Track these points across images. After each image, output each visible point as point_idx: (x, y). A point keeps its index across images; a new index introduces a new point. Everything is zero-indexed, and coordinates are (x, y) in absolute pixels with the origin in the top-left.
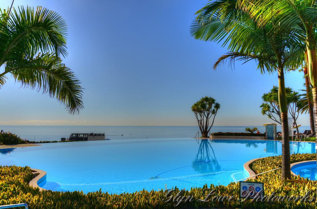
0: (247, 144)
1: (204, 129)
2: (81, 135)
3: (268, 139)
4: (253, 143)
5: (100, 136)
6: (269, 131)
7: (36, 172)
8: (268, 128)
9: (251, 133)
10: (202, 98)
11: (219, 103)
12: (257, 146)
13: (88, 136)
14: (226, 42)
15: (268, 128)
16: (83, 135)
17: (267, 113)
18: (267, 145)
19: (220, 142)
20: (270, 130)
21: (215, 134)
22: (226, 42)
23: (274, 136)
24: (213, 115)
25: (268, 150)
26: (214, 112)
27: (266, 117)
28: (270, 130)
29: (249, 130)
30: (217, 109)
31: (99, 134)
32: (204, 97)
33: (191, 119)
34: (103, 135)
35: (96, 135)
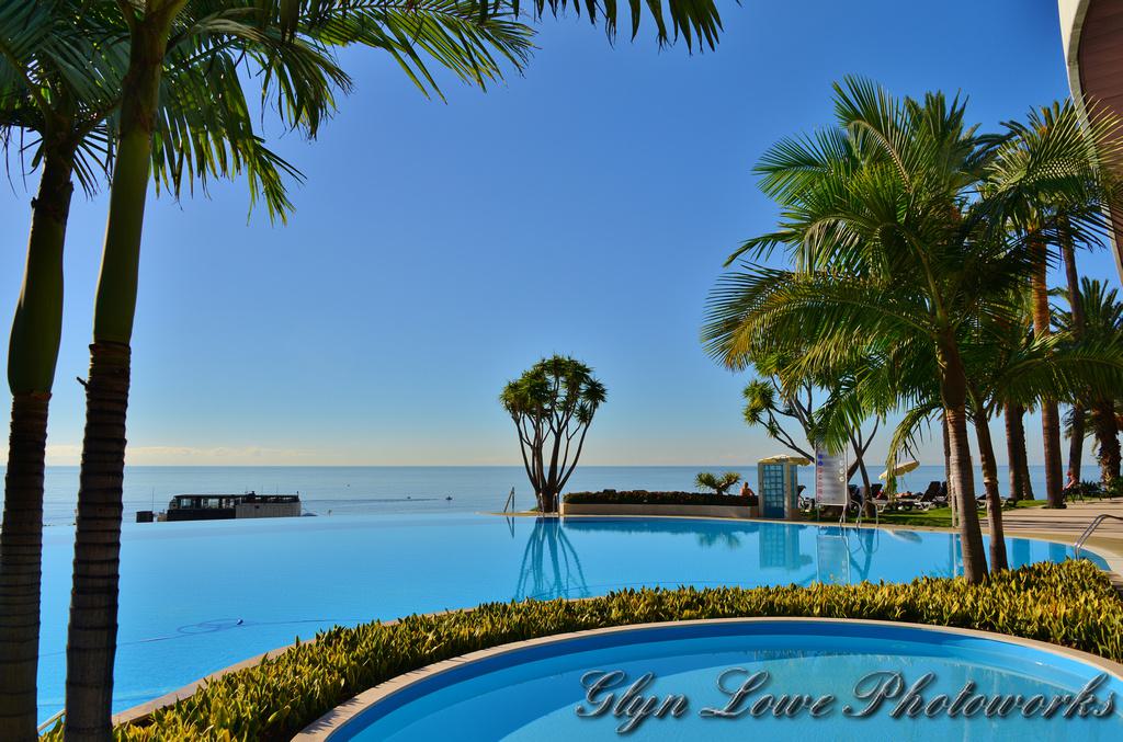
0: (703, 535)
1: (547, 479)
2: (210, 500)
3: (766, 516)
4: (728, 531)
5: (285, 505)
6: (773, 486)
8: (767, 474)
9: (715, 492)
10: (539, 361)
12: (737, 541)
13: (236, 503)
14: (292, 171)
15: (767, 474)
16: (217, 500)
17: (764, 416)
18: (763, 540)
19: (597, 529)
20: (776, 483)
21: (574, 499)
22: (292, 171)
23: (786, 503)
25: (766, 559)
27: (760, 430)
28: (776, 483)
29: (709, 481)
31: (277, 497)
32: (549, 358)
33: (502, 443)
34: (290, 501)
35: (265, 499)
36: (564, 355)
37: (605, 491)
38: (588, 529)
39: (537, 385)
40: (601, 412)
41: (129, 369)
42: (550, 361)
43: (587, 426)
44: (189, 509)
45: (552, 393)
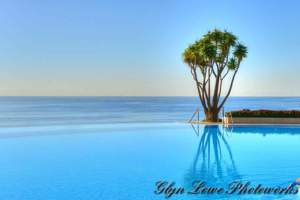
7: (161, 182)
10: (206, 33)
11: (245, 46)
21: (236, 115)
24: (232, 72)
26: (233, 66)
30: (240, 60)
32: (212, 31)
33: (184, 82)
36: (222, 30)
37: (244, 110)
38: (240, 132)
39: (210, 47)
40: (245, 61)
41: (213, 141)
42: (213, 33)
43: (236, 72)
44: (198, 126)
45: (215, 51)
